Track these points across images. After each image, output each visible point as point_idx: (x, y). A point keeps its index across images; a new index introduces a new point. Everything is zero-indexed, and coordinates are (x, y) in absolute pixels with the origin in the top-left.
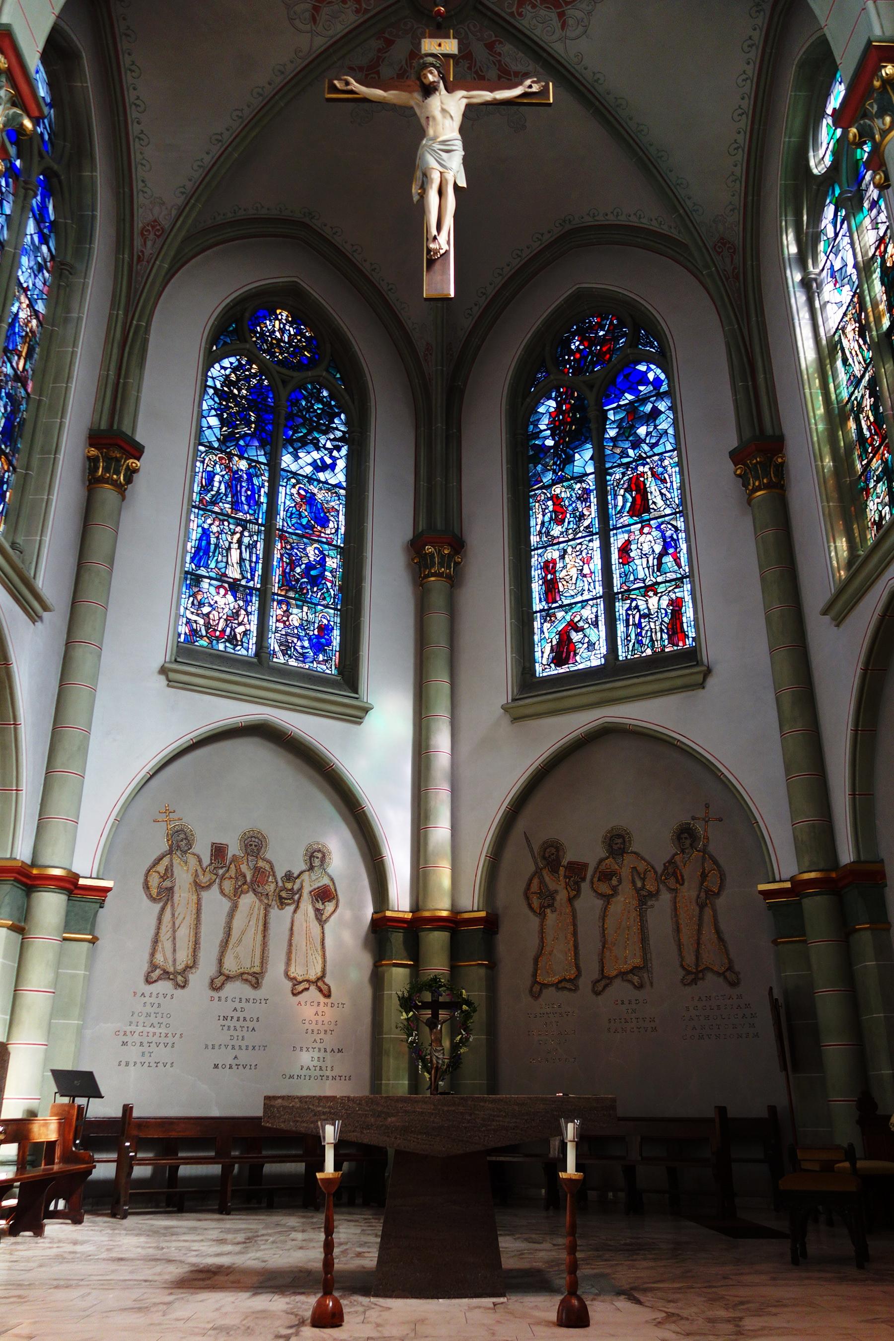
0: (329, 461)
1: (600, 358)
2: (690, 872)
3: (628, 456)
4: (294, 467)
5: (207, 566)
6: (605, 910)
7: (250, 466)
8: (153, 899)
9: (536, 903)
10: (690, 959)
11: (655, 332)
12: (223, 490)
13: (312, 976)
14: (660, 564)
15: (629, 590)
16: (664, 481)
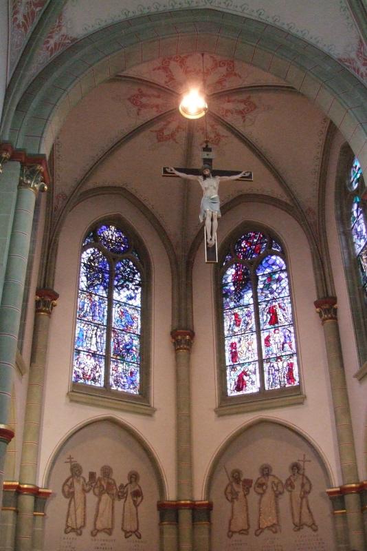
0: (133, 295)
1: (255, 251)
2: (297, 484)
3: (268, 297)
4: (118, 299)
5: (82, 346)
6: (260, 500)
7: (100, 299)
8: (66, 497)
9: (230, 498)
10: (297, 520)
11: (279, 243)
12: (88, 311)
13: (133, 530)
14: (283, 347)
15: (269, 358)
16: (284, 310)
